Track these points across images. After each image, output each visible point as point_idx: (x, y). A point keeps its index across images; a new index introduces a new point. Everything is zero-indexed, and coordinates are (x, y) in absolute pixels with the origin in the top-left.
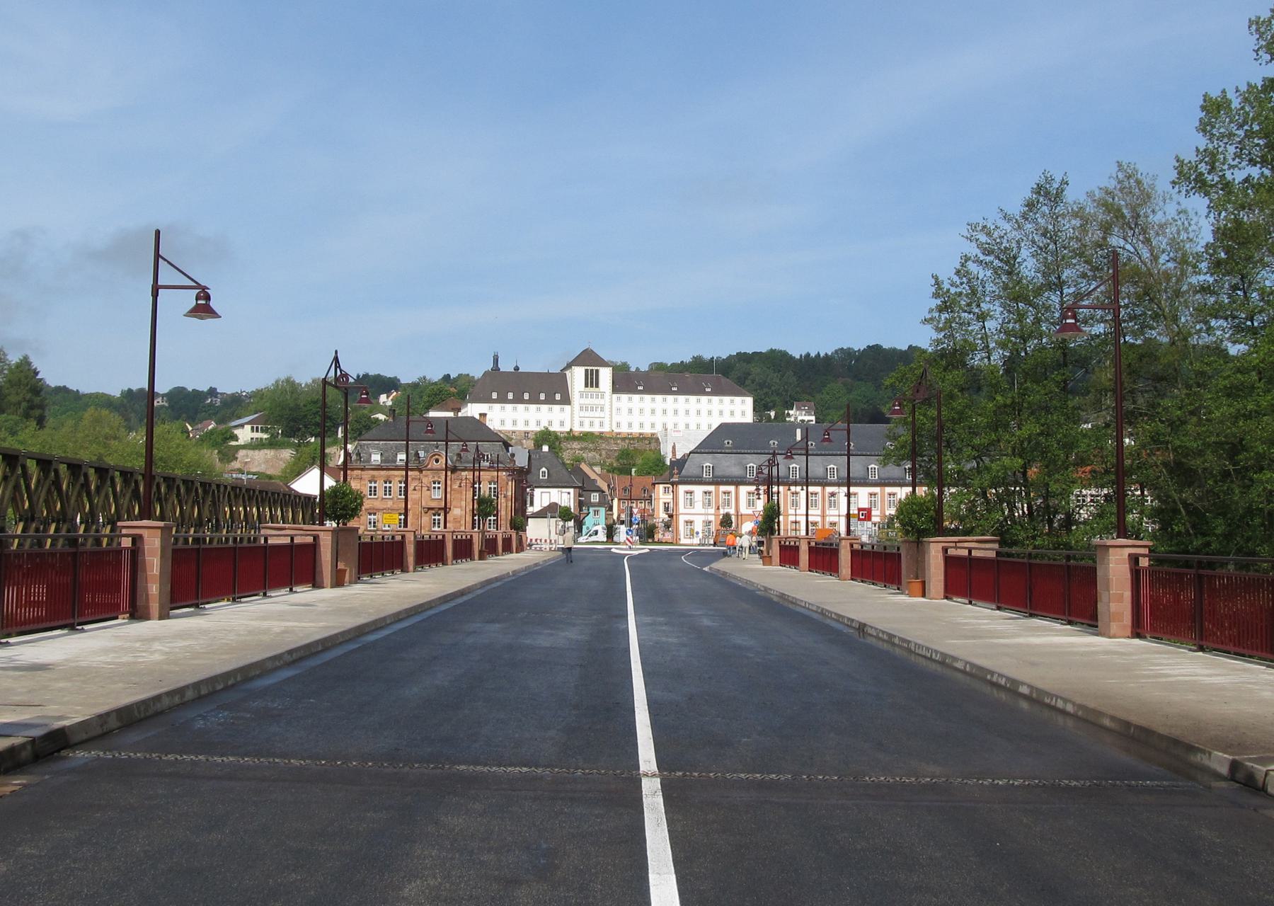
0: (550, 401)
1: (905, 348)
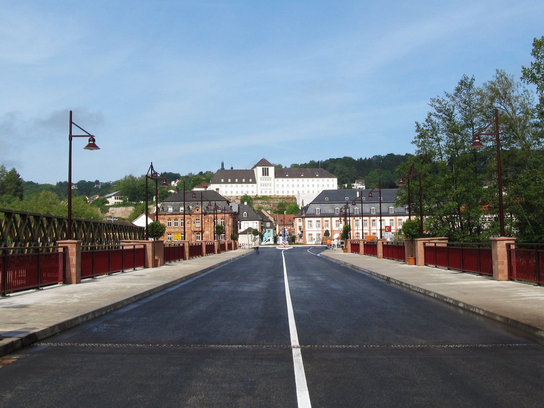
0: (247, 182)
1: (404, 154)
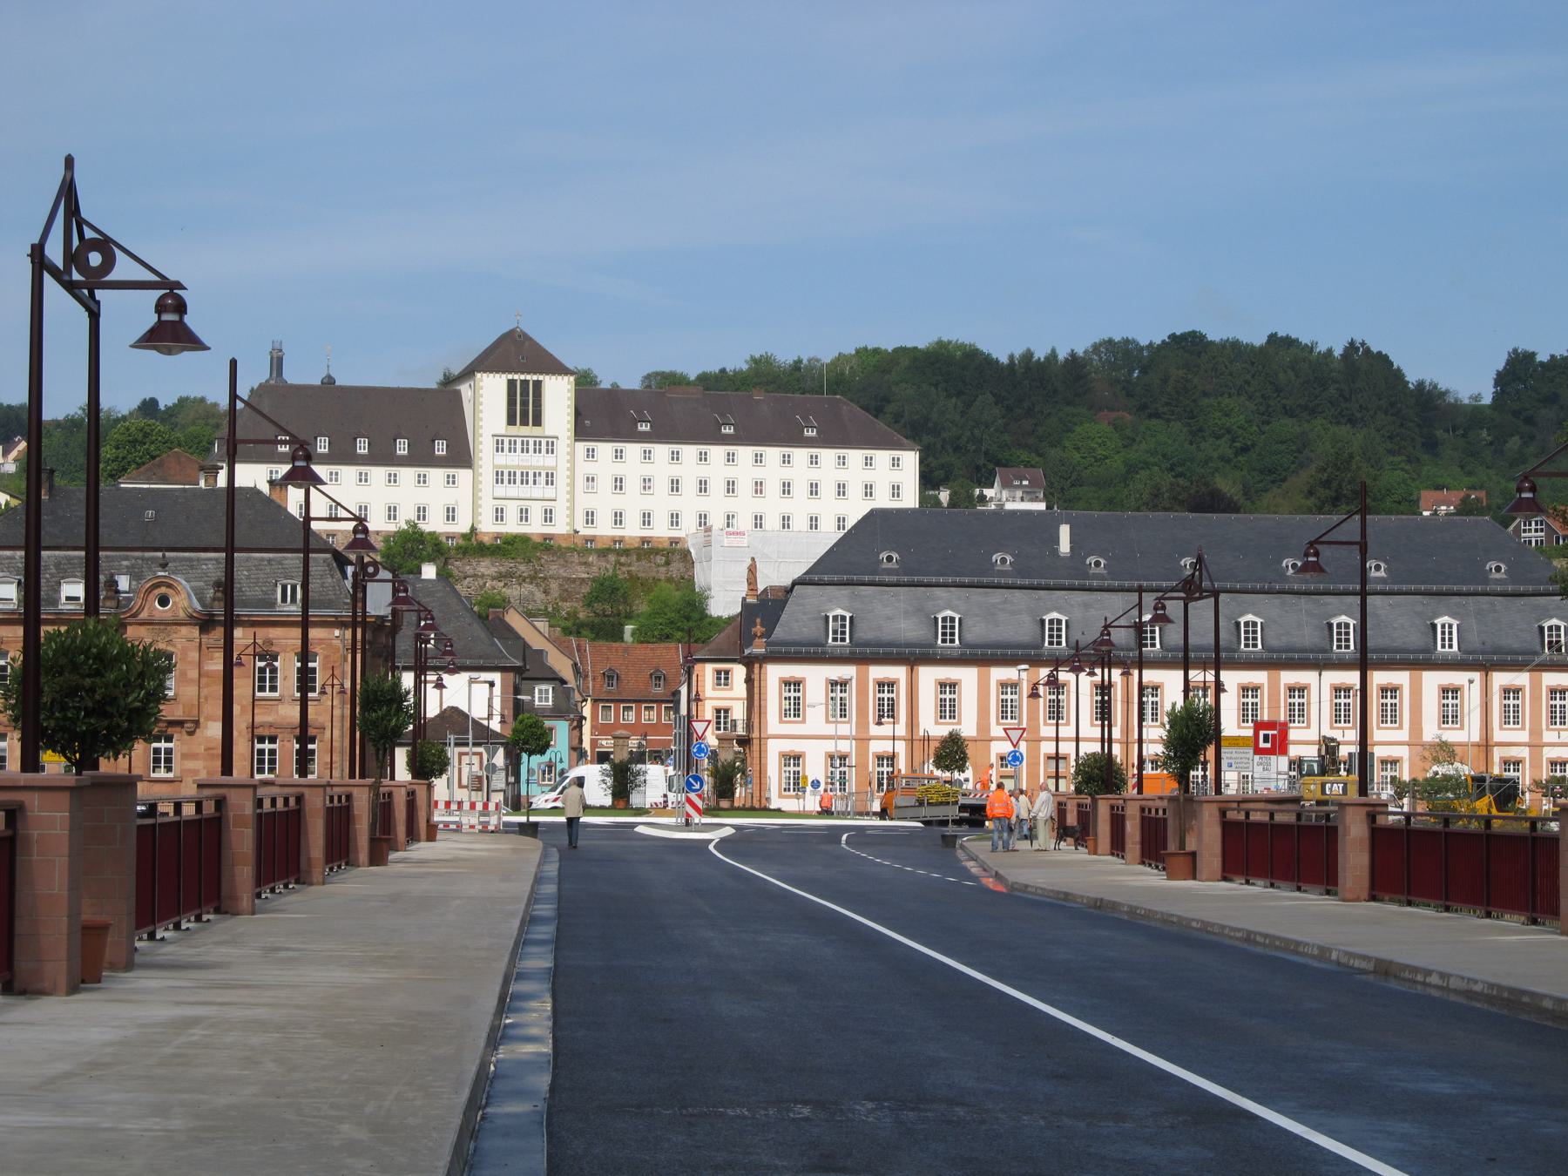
0: (421, 457)
1: (1258, 339)
